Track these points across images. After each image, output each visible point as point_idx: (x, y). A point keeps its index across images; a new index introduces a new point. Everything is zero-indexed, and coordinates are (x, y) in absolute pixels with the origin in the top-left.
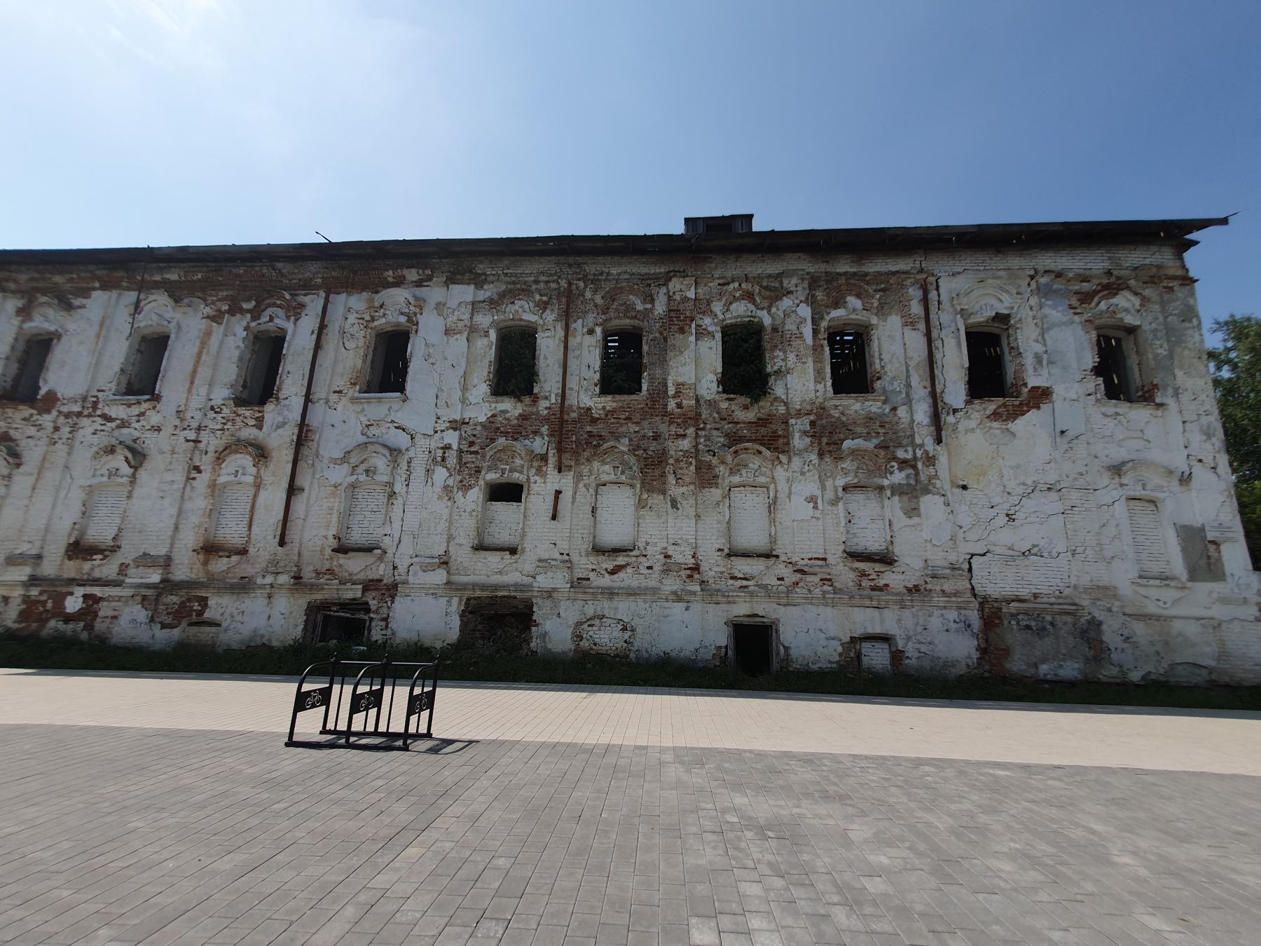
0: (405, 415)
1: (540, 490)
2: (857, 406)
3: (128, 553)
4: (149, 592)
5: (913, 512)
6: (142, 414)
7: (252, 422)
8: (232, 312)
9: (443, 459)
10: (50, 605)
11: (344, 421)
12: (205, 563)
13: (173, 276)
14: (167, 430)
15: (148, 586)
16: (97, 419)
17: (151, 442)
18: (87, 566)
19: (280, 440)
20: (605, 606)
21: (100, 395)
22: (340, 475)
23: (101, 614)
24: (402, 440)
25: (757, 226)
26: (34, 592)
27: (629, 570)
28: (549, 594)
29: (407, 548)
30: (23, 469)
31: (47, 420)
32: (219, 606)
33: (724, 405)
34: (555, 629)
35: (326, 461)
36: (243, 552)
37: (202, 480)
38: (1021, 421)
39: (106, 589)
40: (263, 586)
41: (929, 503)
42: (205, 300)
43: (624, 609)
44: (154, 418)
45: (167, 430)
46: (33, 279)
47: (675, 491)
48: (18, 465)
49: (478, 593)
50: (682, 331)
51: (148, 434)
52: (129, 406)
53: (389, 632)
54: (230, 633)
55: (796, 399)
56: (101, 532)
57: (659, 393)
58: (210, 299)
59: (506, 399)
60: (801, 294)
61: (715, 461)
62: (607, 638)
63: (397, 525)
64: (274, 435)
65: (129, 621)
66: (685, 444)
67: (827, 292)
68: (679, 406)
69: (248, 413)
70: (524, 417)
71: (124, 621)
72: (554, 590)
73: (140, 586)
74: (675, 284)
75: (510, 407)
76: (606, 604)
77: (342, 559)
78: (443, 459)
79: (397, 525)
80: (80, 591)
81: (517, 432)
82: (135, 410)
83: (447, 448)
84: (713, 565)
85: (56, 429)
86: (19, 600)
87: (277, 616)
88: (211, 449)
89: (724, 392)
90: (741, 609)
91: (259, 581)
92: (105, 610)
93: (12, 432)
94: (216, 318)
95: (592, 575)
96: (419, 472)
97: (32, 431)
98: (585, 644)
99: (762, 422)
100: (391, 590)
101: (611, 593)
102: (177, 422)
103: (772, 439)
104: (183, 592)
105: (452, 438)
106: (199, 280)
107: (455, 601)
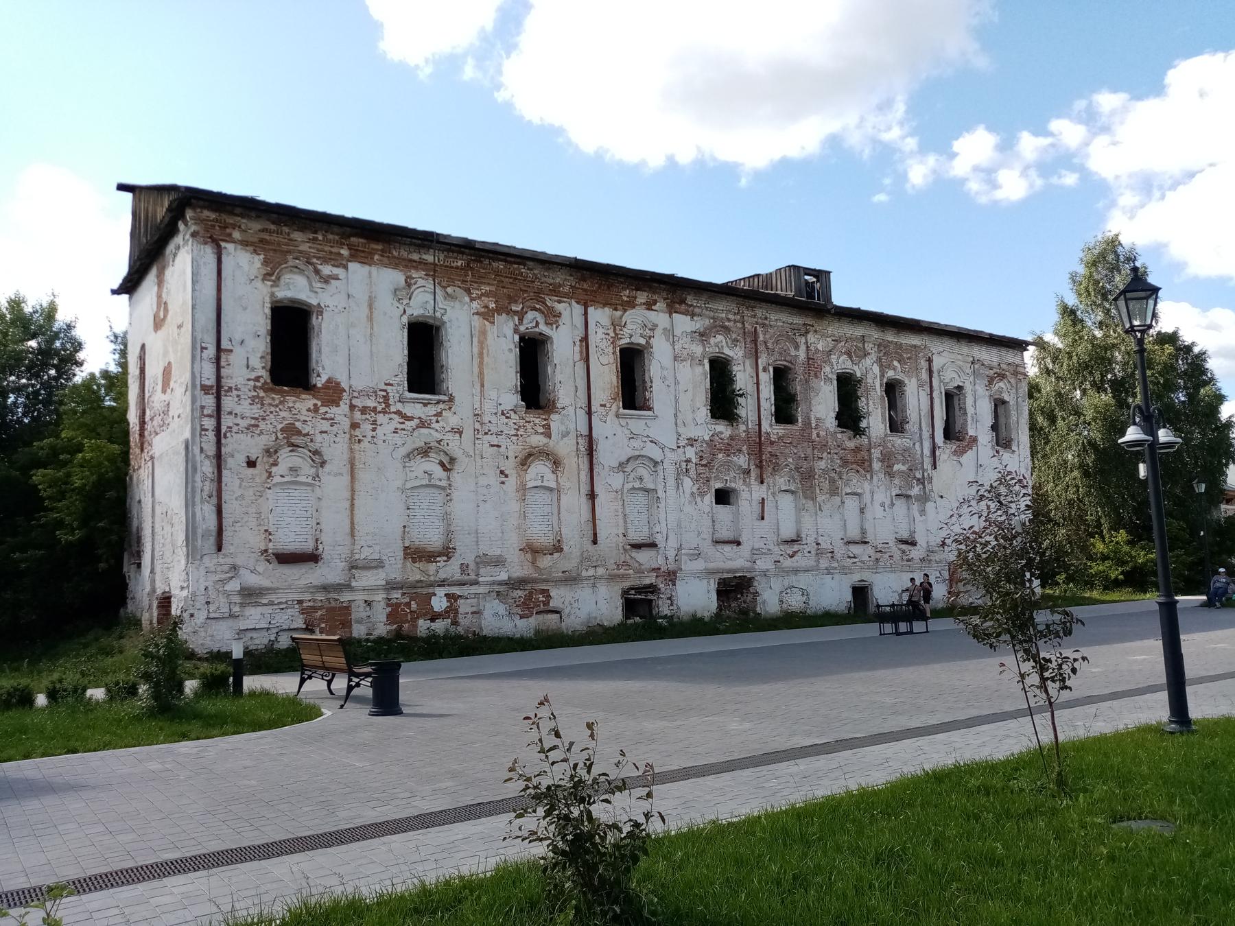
0: (654, 432)
1: (750, 494)
2: (899, 441)
3: (465, 553)
4: (501, 588)
5: (923, 512)
6: (439, 414)
7: (542, 430)
8: (499, 310)
9: (687, 470)
10: (414, 605)
11: (616, 433)
12: (533, 562)
13: (429, 258)
14: (468, 434)
15: (500, 583)
16: (393, 416)
17: (454, 445)
18: (432, 567)
19: (566, 447)
20: (793, 580)
21: (389, 388)
22: (617, 481)
23: (461, 610)
24: (656, 453)
25: (489, 26)
26: (396, 595)
27: (799, 554)
28: (765, 573)
29: (673, 543)
30: (327, 468)
31: (340, 412)
32: (560, 596)
33: (839, 436)
34: (769, 600)
35: (607, 469)
36: (447, 552)
37: (512, 481)
38: (965, 456)
39: (465, 588)
40: (588, 578)
41: (930, 505)
42: (468, 292)
43: (803, 581)
44: (452, 420)
45: (468, 434)
46: (264, 230)
47: (820, 499)
48: (323, 464)
49: (725, 575)
50: (816, 377)
51: (450, 436)
52: (425, 405)
53: (675, 607)
54: (572, 617)
55: (421, 282)
56: (432, 537)
57: (807, 423)
58: (475, 293)
59: (721, 422)
60: (874, 357)
61: (836, 477)
62: (795, 602)
63: (663, 524)
64: (561, 443)
65: (496, 618)
66: (822, 464)
67: (886, 354)
68: (818, 435)
69: (537, 421)
70: (732, 438)
71: (488, 614)
72: (768, 570)
73: (494, 583)
74: (811, 337)
75: (722, 428)
76: (794, 578)
77: (635, 554)
78: (687, 470)
79: (663, 524)
80: (441, 592)
81: (729, 448)
82: (431, 410)
83: (688, 461)
84: (840, 550)
85: (355, 426)
86: (383, 604)
87: (598, 604)
88: (511, 454)
89: (839, 426)
90: (856, 578)
91: (584, 574)
92: (464, 607)
93: (298, 424)
94: (487, 315)
95: (781, 559)
96: (671, 482)
97: (325, 425)
98: (785, 606)
99: (857, 449)
100: (671, 576)
101: (796, 571)
102: (477, 426)
103: (861, 462)
104: (529, 587)
105: (691, 453)
106: (457, 268)
107: (712, 581)
